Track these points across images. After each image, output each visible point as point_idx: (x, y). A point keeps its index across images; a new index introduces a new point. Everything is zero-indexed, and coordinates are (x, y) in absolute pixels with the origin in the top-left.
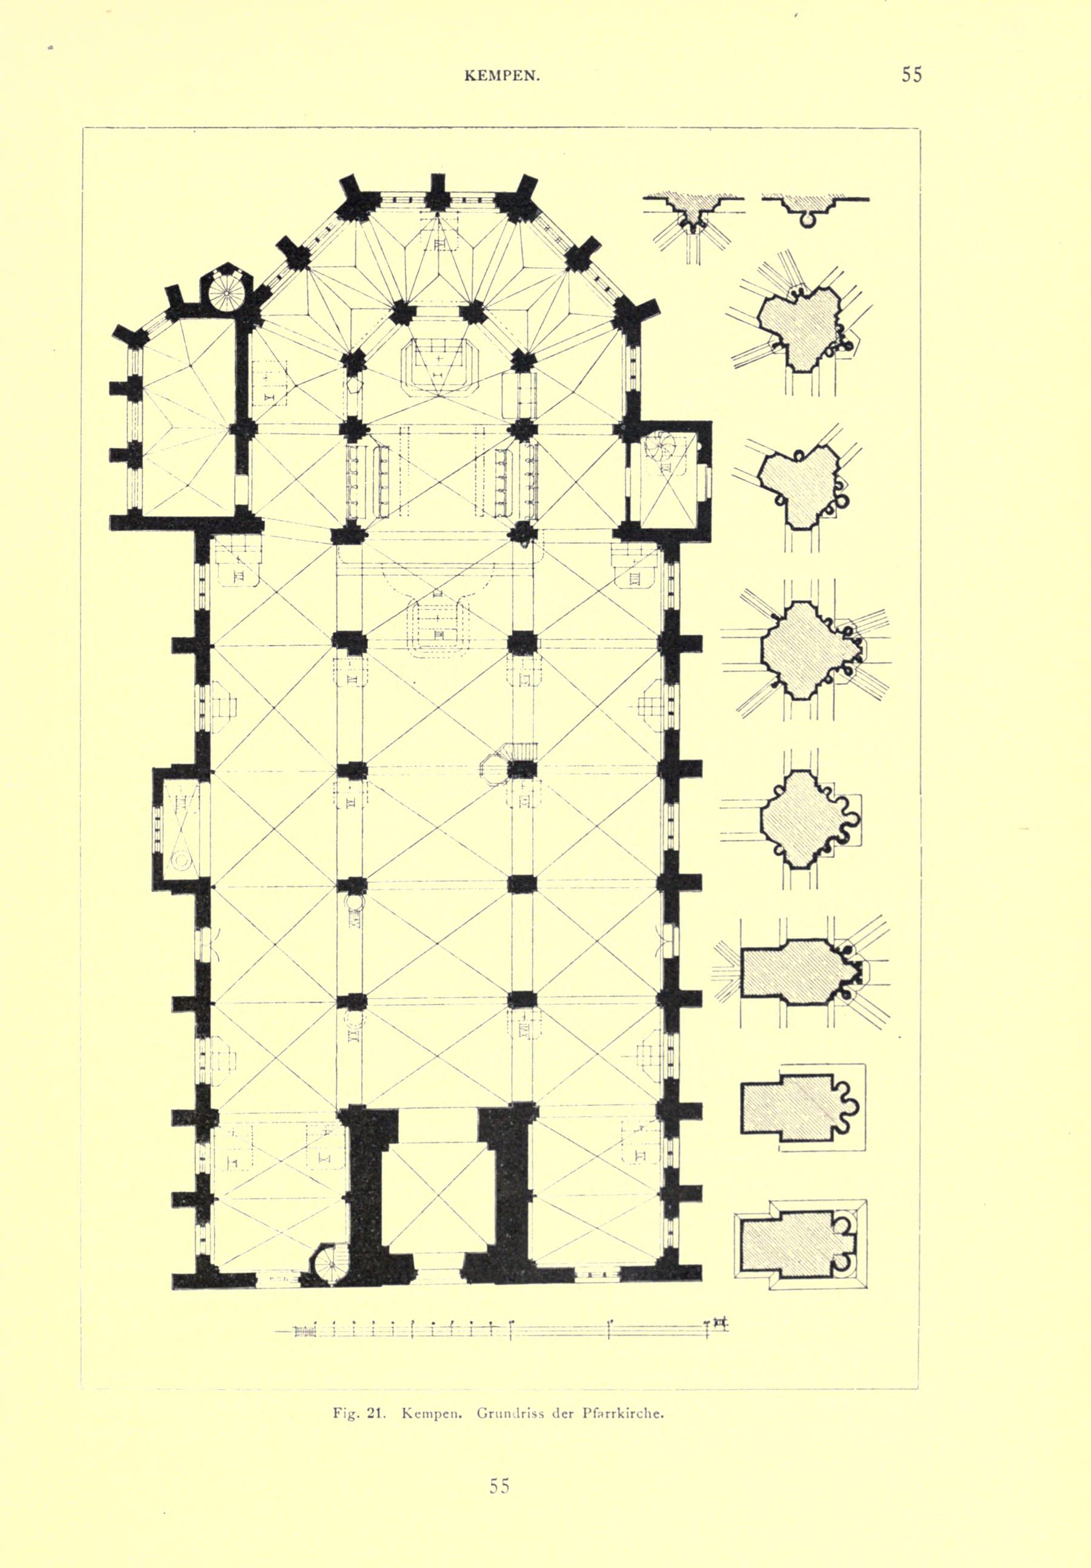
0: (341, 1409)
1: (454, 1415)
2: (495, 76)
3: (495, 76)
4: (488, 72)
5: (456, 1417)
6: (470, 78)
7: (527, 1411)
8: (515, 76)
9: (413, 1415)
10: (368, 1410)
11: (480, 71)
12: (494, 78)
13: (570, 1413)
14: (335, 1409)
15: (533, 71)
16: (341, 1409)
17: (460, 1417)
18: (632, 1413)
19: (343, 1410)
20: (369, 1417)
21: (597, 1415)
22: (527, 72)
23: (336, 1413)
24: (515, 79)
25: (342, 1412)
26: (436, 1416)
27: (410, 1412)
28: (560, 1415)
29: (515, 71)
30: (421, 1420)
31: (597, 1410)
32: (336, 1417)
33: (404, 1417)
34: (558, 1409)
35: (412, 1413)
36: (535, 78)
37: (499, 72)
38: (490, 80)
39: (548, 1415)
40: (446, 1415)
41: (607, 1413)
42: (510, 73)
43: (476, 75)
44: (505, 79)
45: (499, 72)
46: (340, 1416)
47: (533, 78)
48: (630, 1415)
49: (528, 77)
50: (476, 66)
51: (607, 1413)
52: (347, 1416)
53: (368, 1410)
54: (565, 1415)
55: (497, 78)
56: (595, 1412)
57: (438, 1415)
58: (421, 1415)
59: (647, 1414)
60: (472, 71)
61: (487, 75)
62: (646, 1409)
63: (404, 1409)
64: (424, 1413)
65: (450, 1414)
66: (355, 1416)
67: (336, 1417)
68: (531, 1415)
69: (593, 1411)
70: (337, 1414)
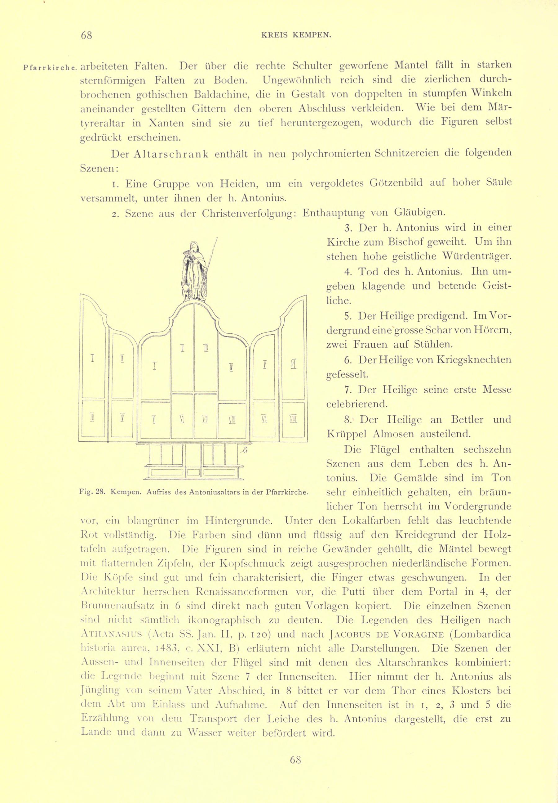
0: (83, 489)
1: (137, 493)
2: (309, 35)
3: (309, 35)
4: (305, 33)
5: (138, 494)
6: (264, 36)
7: (162, 491)
8: (319, 35)
9: (116, 492)
10: (96, 490)
11: (301, 33)
12: (308, 36)
13: (261, 492)
14: (80, 489)
15: (328, 32)
16: (83, 489)
17: (141, 494)
18: (292, 492)
19: (84, 490)
20: (97, 493)
21: (274, 493)
22: (324, 33)
23: (81, 491)
24: (319, 37)
25: (84, 491)
26: (128, 493)
27: (115, 491)
28: (256, 493)
29: (319, 33)
30: (121, 496)
31: (273, 491)
32: (80, 493)
33: (112, 494)
34: (178, 489)
35: (116, 491)
36: (329, 36)
37: (310, 33)
38: (306, 37)
39: (173, 493)
40: (133, 493)
41: (235, 492)
42: (316, 34)
43: (298, 35)
44: (313, 37)
45: (310, 33)
46: (83, 493)
47: (327, 36)
48: (291, 493)
49: (325, 36)
50: (267, 30)
51: (235, 492)
52: (87, 493)
53: (96, 490)
54: (119, 493)
55: (309, 36)
56: (272, 491)
57: (367, 331)
58: (121, 493)
59: (300, 492)
60: (297, 32)
61: (304, 35)
62: (299, 490)
63: (112, 489)
64: (122, 491)
65: (135, 492)
66: (90, 493)
67: (80, 493)
68: (164, 493)
69: (271, 491)
70: (81, 492)
